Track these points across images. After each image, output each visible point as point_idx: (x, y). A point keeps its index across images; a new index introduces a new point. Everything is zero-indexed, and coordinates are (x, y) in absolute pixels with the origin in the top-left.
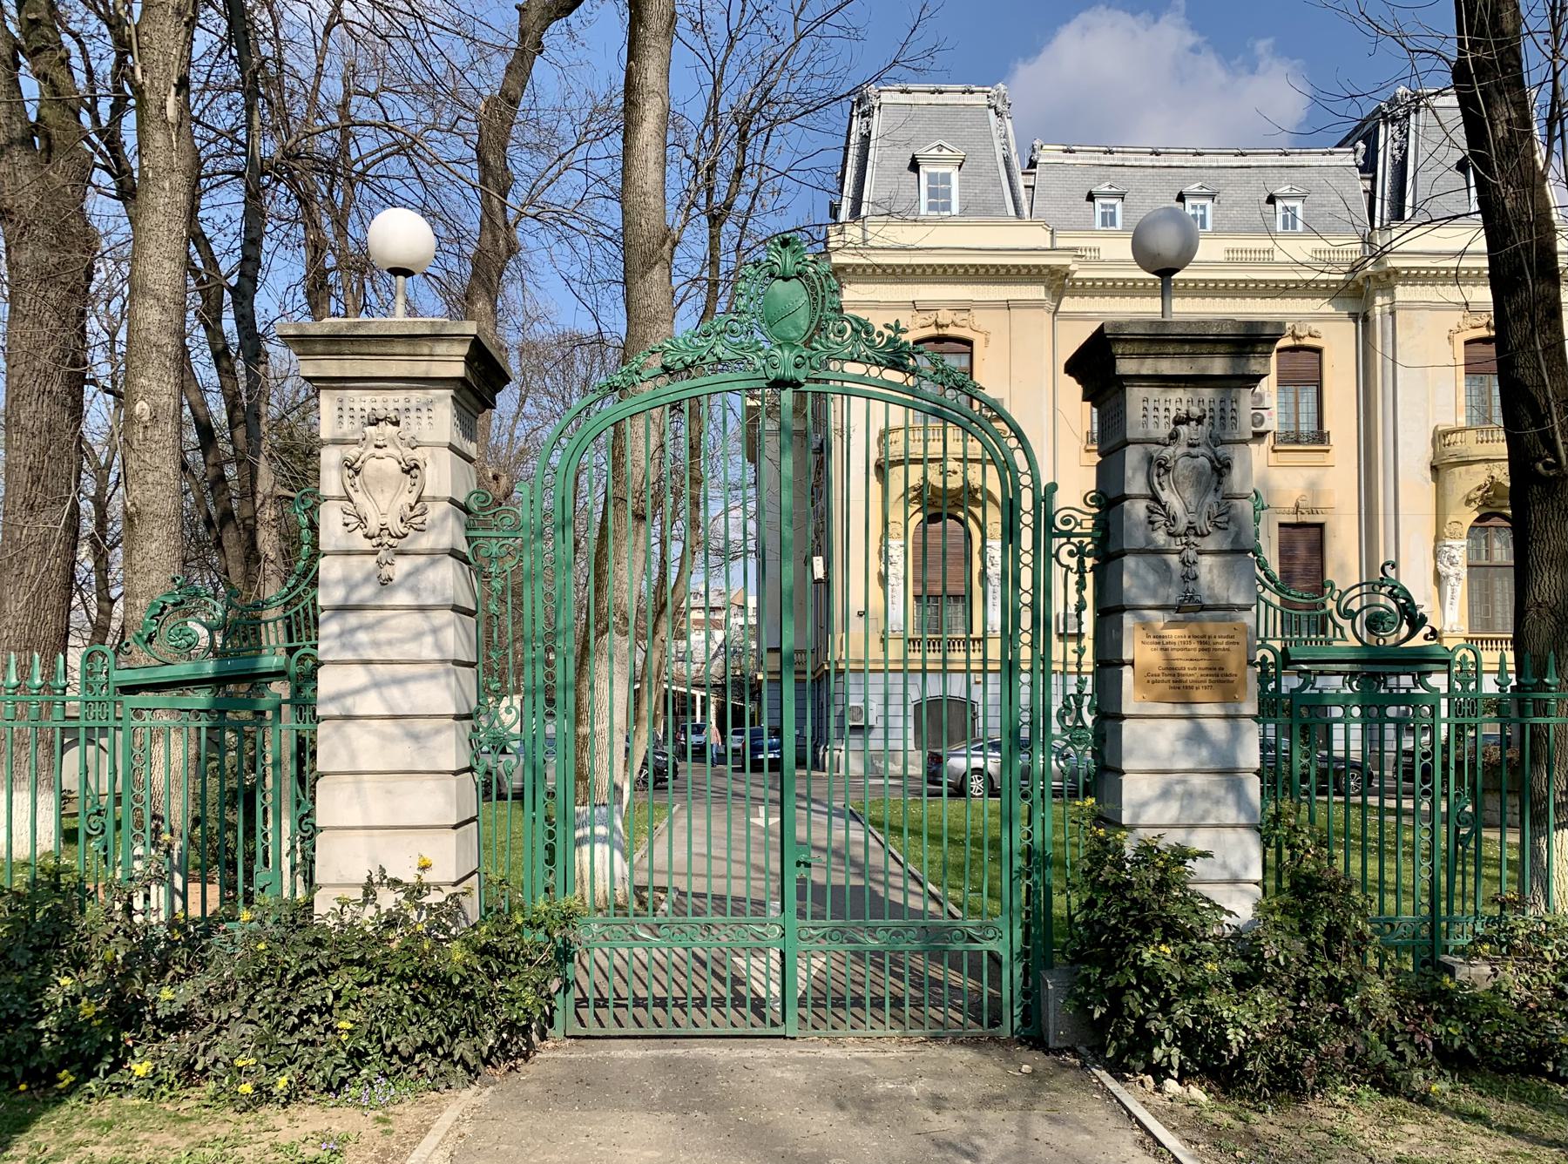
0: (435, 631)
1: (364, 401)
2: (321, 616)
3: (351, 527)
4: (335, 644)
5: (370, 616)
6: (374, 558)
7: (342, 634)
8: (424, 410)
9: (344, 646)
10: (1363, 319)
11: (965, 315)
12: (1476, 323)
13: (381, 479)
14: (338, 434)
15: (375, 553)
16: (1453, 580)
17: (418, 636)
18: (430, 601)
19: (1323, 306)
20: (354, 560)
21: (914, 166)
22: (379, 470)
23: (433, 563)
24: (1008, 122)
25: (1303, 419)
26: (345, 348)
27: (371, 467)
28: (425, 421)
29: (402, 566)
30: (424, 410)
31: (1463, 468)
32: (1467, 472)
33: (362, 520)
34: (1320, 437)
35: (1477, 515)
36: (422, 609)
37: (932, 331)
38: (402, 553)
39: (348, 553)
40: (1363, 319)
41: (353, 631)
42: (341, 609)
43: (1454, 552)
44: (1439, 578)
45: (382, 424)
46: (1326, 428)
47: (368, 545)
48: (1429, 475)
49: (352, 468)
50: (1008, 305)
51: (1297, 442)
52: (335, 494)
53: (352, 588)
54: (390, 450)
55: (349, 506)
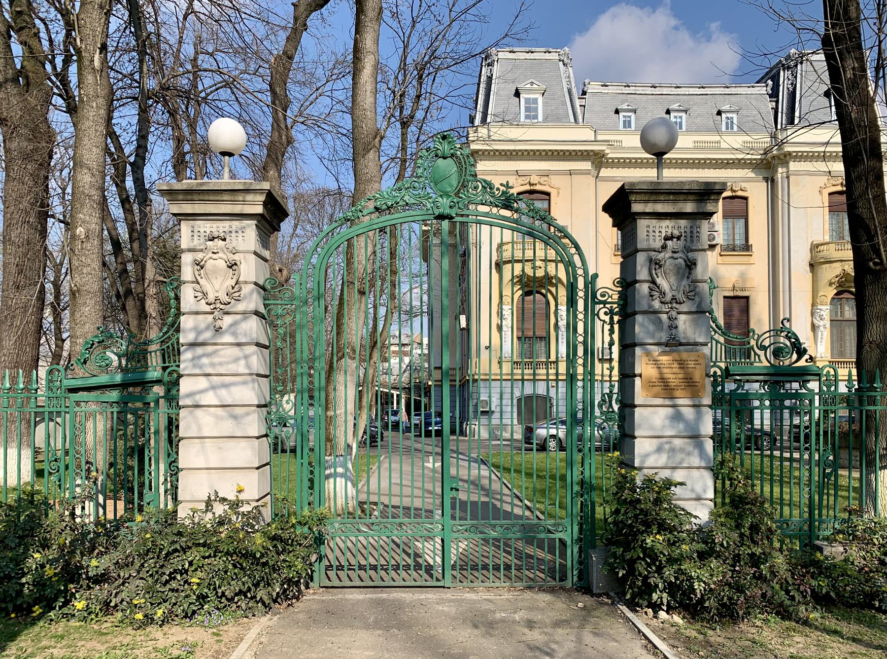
0: (246, 357)
1: (206, 227)
2: (182, 349)
3: (198, 298)
4: (190, 364)
5: (209, 349)
6: (212, 316)
7: (193, 359)
8: (240, 232)
9: (194, 366)
10: (771, 181)
11: (546, 178)
12: (835, 183)
13: (216, 271)
14: (191, 246)
15: (212, 313)
16: (822, 328)
17: (236, 360)
18: (244, 340)
19: (748, 173)
20: (200, 317)
21: (517, 94)
22: (214, 266)
23: (245, 319)
24: (570, 69)
25: (737, 237)
26: (195, 197)
27: (210, 264)
28: (240, 238)
29: (228, 320)
30: (240, 232)
31: (828, 265)
32: (830, 267)
33: (205, 294)
34: (747, 247)
35: (835, 291)
36: (239, 345)
37: (527, 188)
38: (227, 313)
39: (197, 313)
40: (771, 181)
41: (200, 357)
42: (193, 345)
43: (822, 313)
44: (814, 327)
45: (216, 240)
46: (750, 243)
47: (208, 308)
48: (808, 269)
49: (199, 265)
50: (570, 173)
51: (734, 250)
52: (190, 280)
53: (199, 333)
54: (221, 255)
55: (197, 287)
